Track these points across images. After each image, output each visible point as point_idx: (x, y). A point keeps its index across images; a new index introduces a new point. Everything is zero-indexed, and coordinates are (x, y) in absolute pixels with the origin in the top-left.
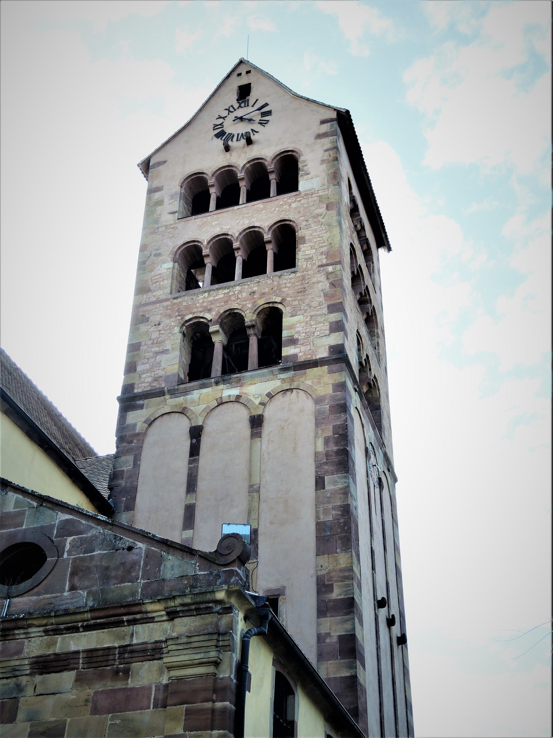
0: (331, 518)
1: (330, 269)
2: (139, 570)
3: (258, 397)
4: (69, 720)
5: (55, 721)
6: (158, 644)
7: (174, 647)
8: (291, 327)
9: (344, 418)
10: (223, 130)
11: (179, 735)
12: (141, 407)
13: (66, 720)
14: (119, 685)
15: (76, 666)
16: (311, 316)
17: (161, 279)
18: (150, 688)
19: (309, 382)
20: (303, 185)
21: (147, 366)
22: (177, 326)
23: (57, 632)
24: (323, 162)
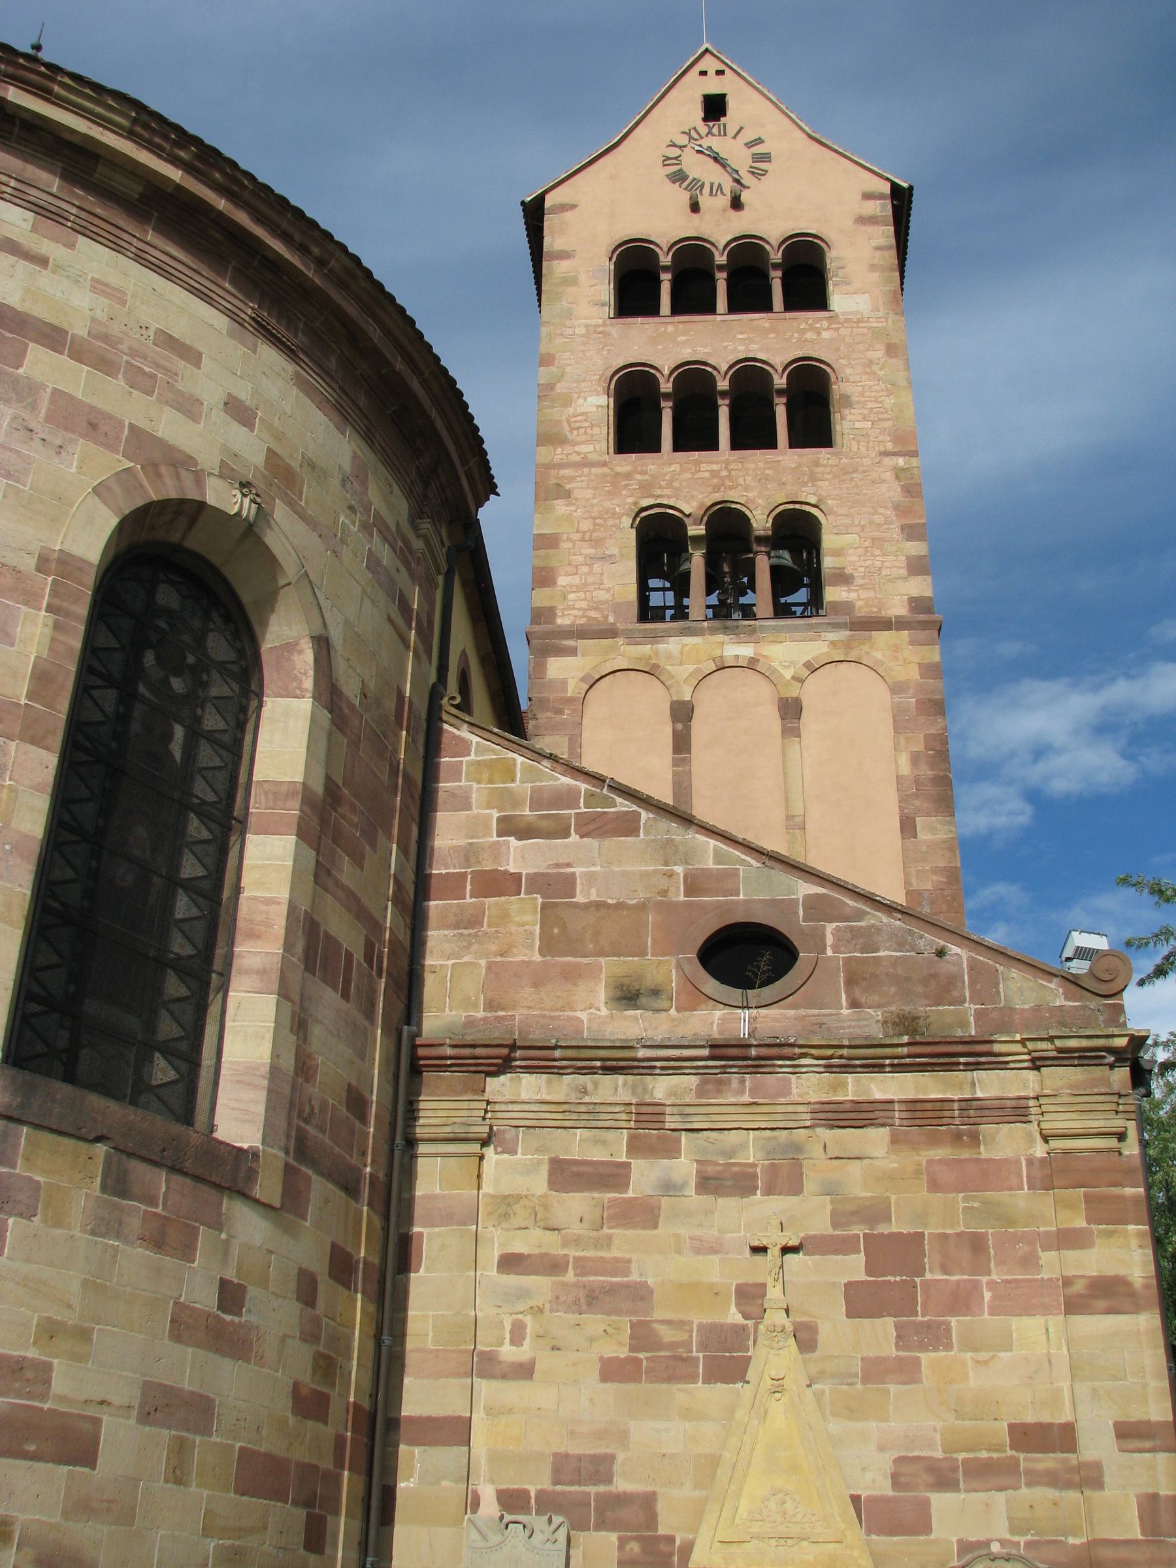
0: (929, 886)
1: (901, 462)
2: (964, 988)
3: (788, 667)
4: (893, 1198)
5: (871, 1197)
6: (1022, 1102)
7: (1052, 1108)
8: (838, 553)
9: (942, 725)
10: (681, 170)
11: (1081, 1229)
12: (573, 652)
13: (889, 1199)
14: (966, 1154)
15: (890, 1121)
16: (873, 540)
17: (587, 424)
18: (1018, 1162)
19: (878, 655)
20: (837, 300)
21: (576, 580)
22: (627, 515)
23: (846, 1068)
24: (872, 268)
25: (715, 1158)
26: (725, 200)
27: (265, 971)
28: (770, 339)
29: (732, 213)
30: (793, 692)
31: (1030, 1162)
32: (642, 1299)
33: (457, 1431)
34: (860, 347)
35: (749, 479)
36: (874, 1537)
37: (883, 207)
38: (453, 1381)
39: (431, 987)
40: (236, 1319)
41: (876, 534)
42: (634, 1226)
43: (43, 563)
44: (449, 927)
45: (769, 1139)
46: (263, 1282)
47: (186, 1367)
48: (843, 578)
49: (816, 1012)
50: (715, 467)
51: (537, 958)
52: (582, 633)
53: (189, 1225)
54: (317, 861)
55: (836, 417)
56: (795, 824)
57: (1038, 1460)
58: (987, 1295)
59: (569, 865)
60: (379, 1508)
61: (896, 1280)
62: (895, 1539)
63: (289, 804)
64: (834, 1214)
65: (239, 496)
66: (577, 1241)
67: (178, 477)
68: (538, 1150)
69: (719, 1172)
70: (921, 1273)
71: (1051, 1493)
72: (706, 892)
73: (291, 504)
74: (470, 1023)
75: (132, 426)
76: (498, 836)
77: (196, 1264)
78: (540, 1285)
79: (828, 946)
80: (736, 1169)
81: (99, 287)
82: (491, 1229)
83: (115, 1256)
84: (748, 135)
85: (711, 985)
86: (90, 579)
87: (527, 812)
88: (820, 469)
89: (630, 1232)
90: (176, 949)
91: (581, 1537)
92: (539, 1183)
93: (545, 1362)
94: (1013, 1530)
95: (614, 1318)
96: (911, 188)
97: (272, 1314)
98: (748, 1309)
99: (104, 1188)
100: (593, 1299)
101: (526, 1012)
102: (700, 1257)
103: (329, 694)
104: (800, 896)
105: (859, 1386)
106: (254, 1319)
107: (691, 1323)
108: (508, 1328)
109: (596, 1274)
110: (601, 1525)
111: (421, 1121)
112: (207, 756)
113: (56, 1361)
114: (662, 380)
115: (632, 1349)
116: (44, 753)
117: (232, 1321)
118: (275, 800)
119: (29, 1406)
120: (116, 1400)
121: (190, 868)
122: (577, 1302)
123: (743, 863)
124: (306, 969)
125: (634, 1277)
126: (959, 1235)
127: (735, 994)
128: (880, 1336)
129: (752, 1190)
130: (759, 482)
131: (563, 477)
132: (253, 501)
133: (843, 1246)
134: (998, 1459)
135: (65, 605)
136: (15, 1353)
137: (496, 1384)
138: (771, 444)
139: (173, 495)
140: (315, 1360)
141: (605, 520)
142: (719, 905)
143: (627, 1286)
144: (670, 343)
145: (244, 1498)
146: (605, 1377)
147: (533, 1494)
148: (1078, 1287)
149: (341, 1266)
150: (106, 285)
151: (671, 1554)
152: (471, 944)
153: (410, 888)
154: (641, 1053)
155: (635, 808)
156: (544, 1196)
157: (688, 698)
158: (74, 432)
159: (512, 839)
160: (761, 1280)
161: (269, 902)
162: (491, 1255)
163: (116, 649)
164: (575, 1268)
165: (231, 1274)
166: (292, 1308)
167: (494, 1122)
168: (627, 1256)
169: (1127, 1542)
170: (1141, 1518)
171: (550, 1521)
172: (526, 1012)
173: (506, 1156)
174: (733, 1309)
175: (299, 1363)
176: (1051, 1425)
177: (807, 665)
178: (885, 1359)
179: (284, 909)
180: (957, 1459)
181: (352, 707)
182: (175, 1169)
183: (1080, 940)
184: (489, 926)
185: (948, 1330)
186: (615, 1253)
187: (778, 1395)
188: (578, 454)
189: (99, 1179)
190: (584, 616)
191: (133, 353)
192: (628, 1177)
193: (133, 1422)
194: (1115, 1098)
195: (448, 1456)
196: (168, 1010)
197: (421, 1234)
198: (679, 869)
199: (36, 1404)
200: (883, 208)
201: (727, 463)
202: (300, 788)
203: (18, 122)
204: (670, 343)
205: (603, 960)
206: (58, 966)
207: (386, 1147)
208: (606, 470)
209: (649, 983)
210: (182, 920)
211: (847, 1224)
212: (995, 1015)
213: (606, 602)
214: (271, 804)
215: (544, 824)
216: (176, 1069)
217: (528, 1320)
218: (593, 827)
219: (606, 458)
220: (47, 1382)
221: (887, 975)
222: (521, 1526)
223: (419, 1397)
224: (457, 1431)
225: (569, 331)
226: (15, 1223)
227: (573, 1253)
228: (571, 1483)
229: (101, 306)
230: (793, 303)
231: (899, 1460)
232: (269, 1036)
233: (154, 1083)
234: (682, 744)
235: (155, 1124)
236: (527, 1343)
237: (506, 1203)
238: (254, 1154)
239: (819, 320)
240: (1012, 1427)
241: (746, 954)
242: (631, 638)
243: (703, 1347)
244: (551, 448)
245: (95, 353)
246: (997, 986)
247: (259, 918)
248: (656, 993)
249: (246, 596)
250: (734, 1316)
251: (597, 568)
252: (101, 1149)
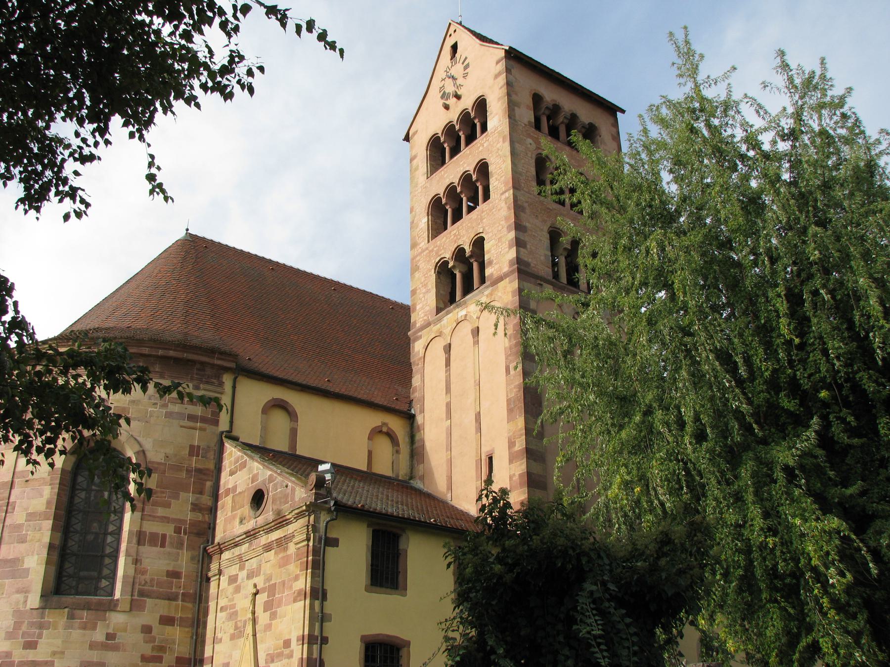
12: (420, 337)
29: (459, 102)
154: (237, 539)
182: (89, 609)
249: (120, 449)
252: (66, 610)
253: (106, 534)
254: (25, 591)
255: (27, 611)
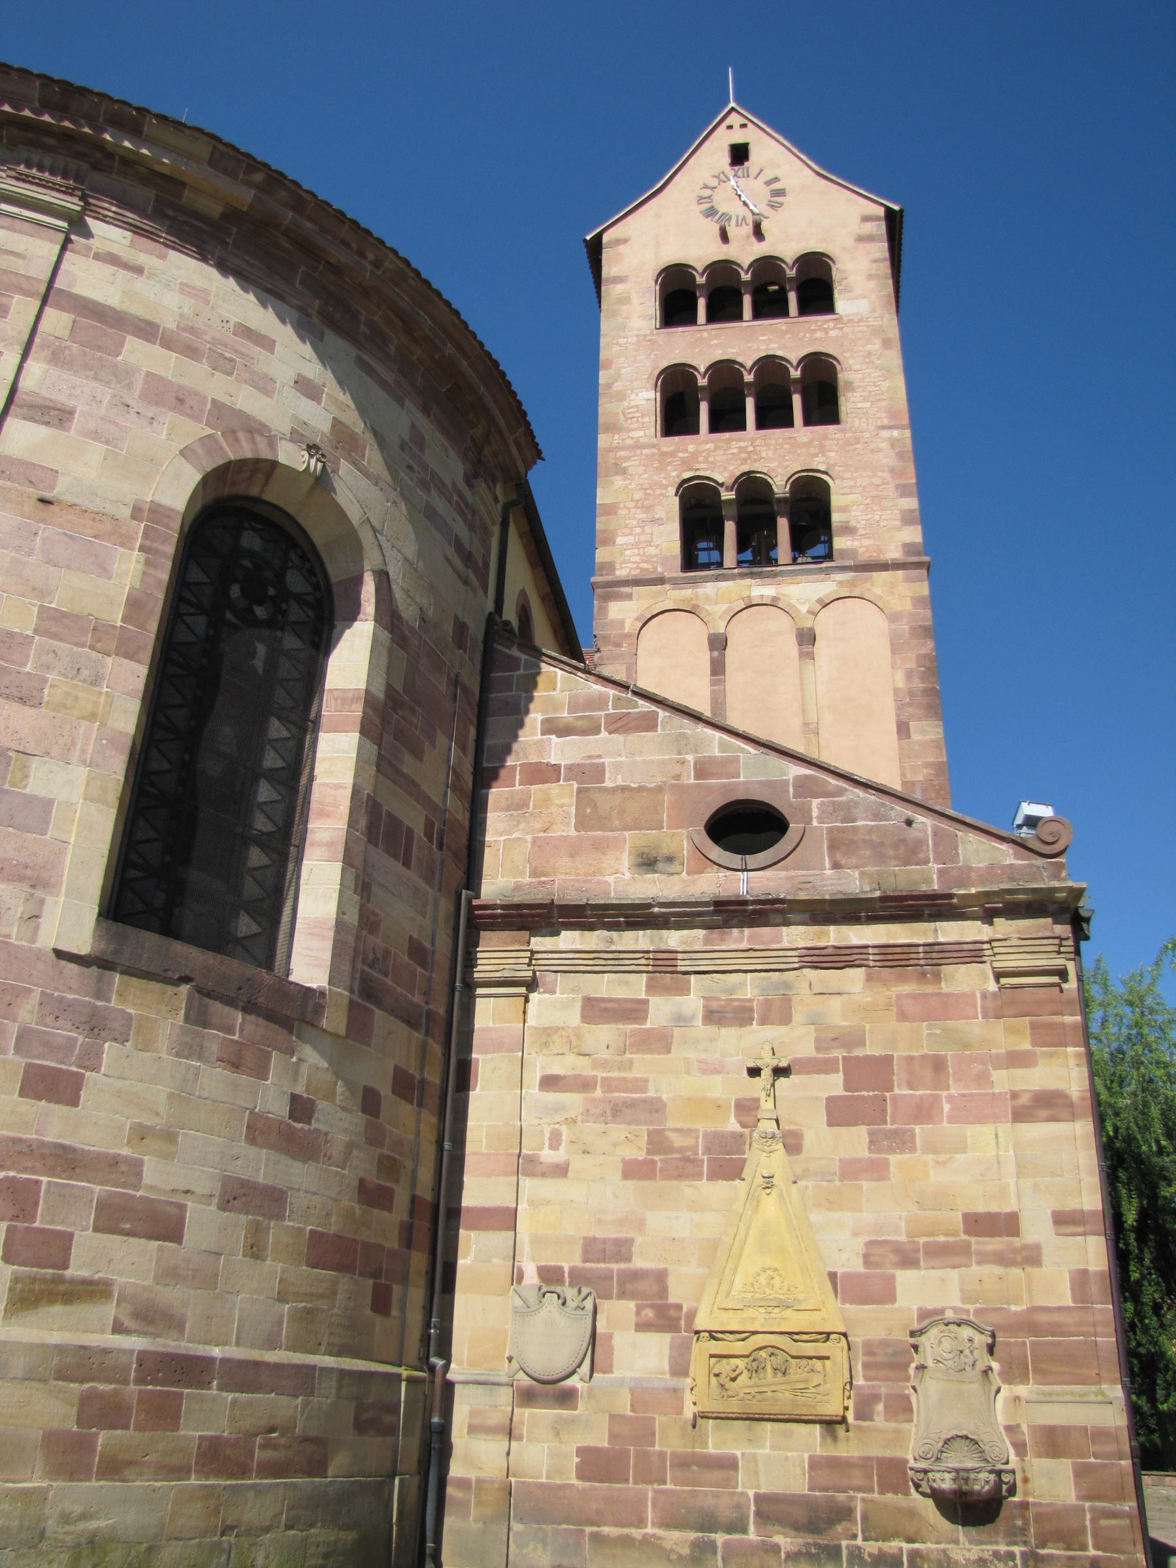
4: (868, 1026)
6: (978, 946)
8: (844, 509)
11: (1027, 1052)
12: (629, 597)
14: (929, 989)
18: (973, 995)
19: (878, 591)
20: (842, 304)
21: (631, 539)
24: (870, 277)
25: (718, 995)
26: (749, 229)
27: (332, 843)
28: (788, 339)
30: (807, 623)
31: (984, 996)
32: (657, 1111)
33: (506, 1219)
34: (861, 342)
35: (770, 453)
36: (848, 1306)
37: (878, 227)
38: (502, 1179)
39: (489, 858)
40: (306, 1127)
41: (876, 493)
42: (651, 1052)
43: (137, 513)
44: (502, 810)
45: (764, 978)
46: (330, 1096)
47: (261, 1166)
48: (848, 530)
49: (804, 872)
50: (742, 444)
51: (573, 832)
52: (637, 582)
53: (262, 1050)
54: (379, 753)
55: (842, 400)
56: (811, 730)
57: (986, 1243)
58: (946, 1107)
59: (599, 756)
60: (442, 1280)
61: (869, 1094)
62: (866, 1307)
63: (353, 707)
64: (817, 1040)
65: (307, 456)
66: (604, 1065)
67: (253, 441)
68: (573, 990)
69: (722, 1006)
70: (890, 1088)
71: (997, 1270)
72: (712, 775)
73: (354, 463)
74: (518, 888)
75: (214, 401)
76: (543, 734)
77: (269, 1082)
78: (573, 1100)
79: (813, 818)
80: (736, 1004)
81: (186, 289)
82: (534, 1055)
83: (197, 1074)
84: (768, 175)
85: (716, 852)
86: (177, 524)
87: (565, 714)
88: (828, 443)
89: (648, 1057)
90: (259, 826)
91: (605, 1306)
92: (573, 1017)
93: (578, 1163)
94: (966, 1299)
95: (634, 1127)
96: (901, 211)
97: (337, 1121)
98: (745, 1119)
99: (187, 1018)
100: (617, 1112)
101: (563, 877)
102: (705, 1077)
103: (388, 616)
104: (791, 777)
105: (837, 1183)
106: (321, 1127)
107: (697, 1131)
108: (547, 1135)
109: (620, 1091)
110: (622, 1295)
111: (479, 968)
112: (285, 668)
113: (146, 1158)
114: (699, 377)
115: (649, 1152)
116: (135, 665)
117: (302, 1128)
118: (343, 705)
119: (125, 1194)
120: (198, 1190)
121: (271, 760)
122: (604, 1114)
123: (743, 750)
124: (369, 841)
125: (651, 1094)
126: (923, 1057)
127: (735, 860)
128: (855, 1141)
129: (750, 1021)
130: (775, 455)
131: (620, 458)
132: (318, 460)
133: (827, 1067)
134: (954, 1242)
135: (155, 545)
136: (111, 1151)
137: (537, 1181)
138: (789, 423)
139: (249, 455)
140: (380, 1162)
141: (654, 490)
142: (724, 786)
143: (645, 1101)
144: (704, 345)
145: (315, 1270)
146: (627, 1175)
147: (566, 1270)
148: (1024, 1100)
149: (404, 1085)
150: (193, 288)
151: (679, 1319)
152: (519, 823)
153: (469, 779)
155: (653, 708)
156: (578, 1028)
157: (722, 631)
158: (164, 406)
159: (553, 737)
160: (755, 1095)
161: (337, 787)
162: (533, 1077)
163: (205, 584)
164: (602, 1087)
165: (300, 1090)
166: (358, 1119)
167: (537, 968)
168: (645, 1076)
169: (1060, 1309)
170: (1072, 1290)
171: (580, 1292)
172: (563, 877)
173: (547, 995)
174: (733, 1120)
175: (363, 1165)
176: (998, 1215)
177: (819, 601)
178: (859, 1161)
179: (349, 792)
180: (918, 1243)
181: (412, 629)
183: (1029, 809)
184: (534, 807)
185: (913, 1136)
186: (636, 1073)
187: (768, 1191)
188: (632, 438)
189: (182, 1012)
190: (637, 568)
191: (215, 341)
192: (647, 1011)
193: (213, 1208)
194: (1057, 941)
195: (499, 1239)
196: (252, 876)
197: (477, 1060)
198: (690, 758)
199: (130, 1191)
200: (880, 228)
201: (753, 440)
202: (363, 694)
203: (117, 158)
204: (704, 345)
205: (627, 834)
206: (155, 840)
207: (446, 989)
208: (654, 451)
209: (665, 850)
210: (264, 803)
211: (829, 1048)
212: (955, 873)
213: (656, 555)
214: (339, 708)
215: (580, 723)
216: (259, 925)
217: (564, 1129)
218: (619, 725)
219: (655, 441)
220: (139, 1174)
221: (864, 841)
222: (555, 1296)
223: (477, 1191)
224: (506, 1219)
225: (622, 341)
226: (110, 1046)
227: (600, 1074)
228: (598, 1261)
229: (188, 305)
230: (806, 308)
231: (871, 1244)
232: (336, 895)
233: (240, 935)
234: (718, 668)
235: (234, 968)
236: (562, 1147)
237: (547, 1034)
238: (322, 993)
239: (826, 321)
240: (966, 1216)
241: (746, 826)
242: (675, 582)
243: (708, 1150)
244: (610, 435)
245: (182, 343)
246: (956, 848)
247: (329, 800)
248: (670, 859)
250: (733, 1125)
251: (648, 529)
252: (185, 989)
253: (257, 774)
254: (37, 880)
255: (39, 955)
